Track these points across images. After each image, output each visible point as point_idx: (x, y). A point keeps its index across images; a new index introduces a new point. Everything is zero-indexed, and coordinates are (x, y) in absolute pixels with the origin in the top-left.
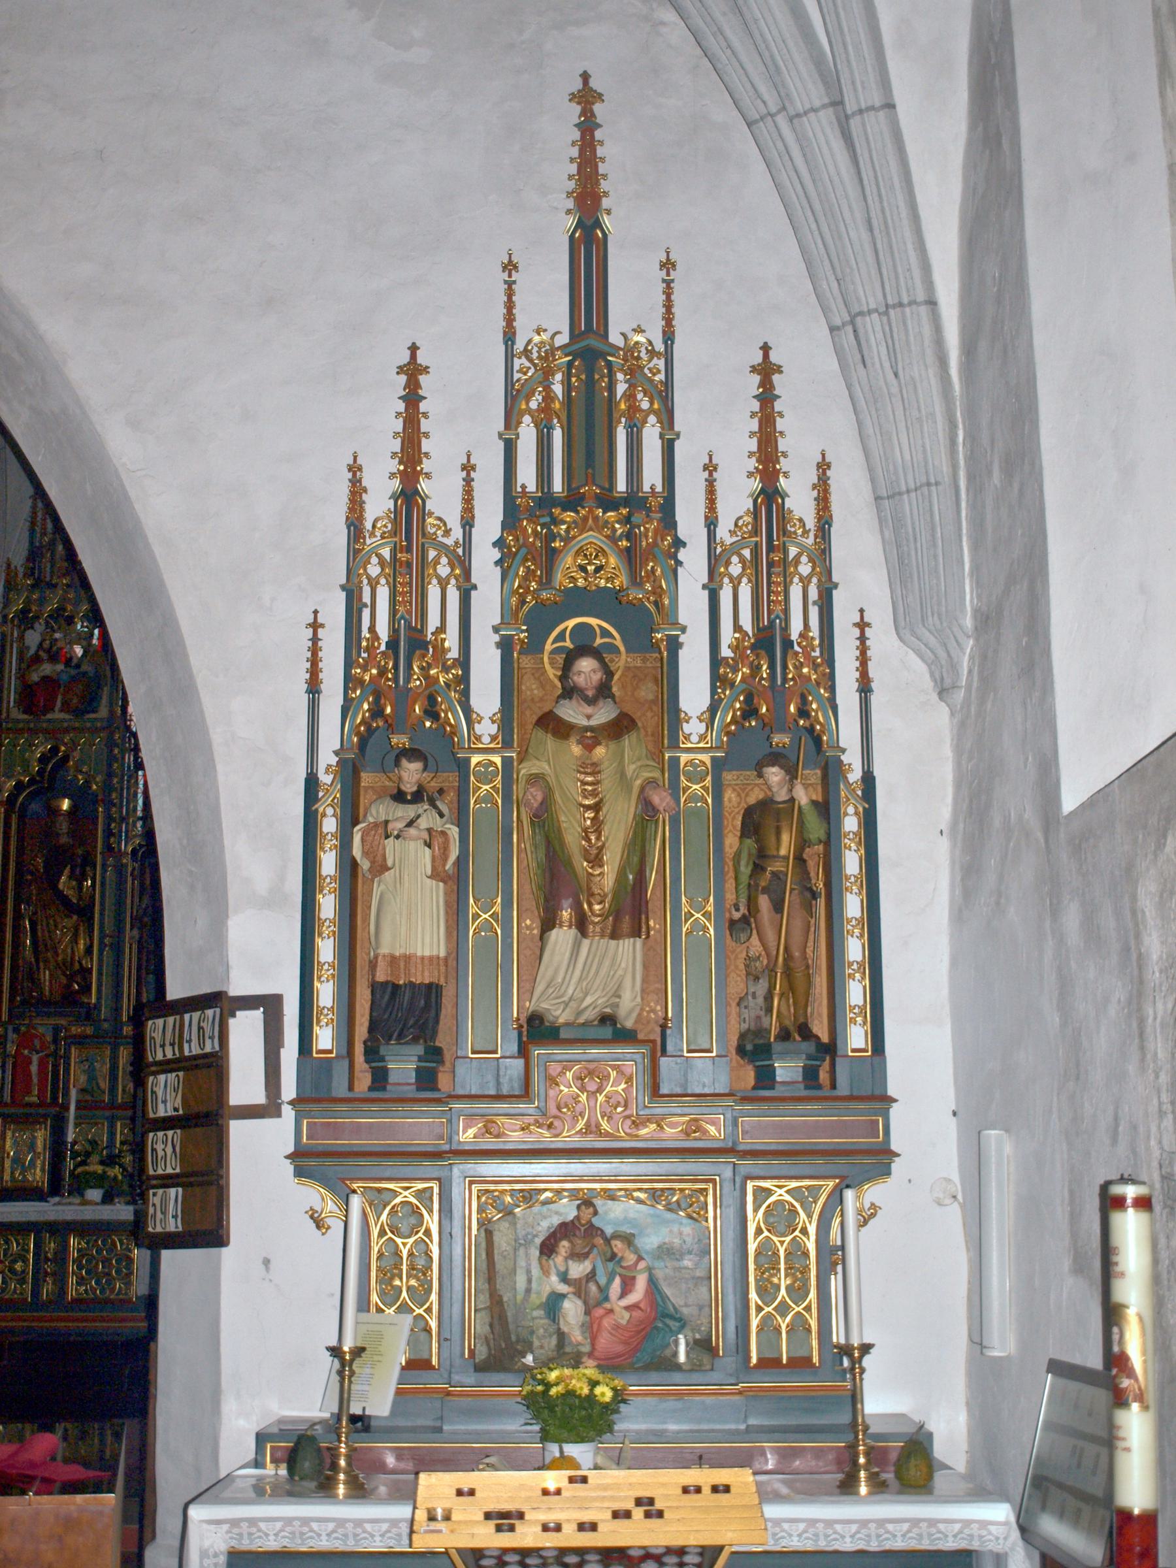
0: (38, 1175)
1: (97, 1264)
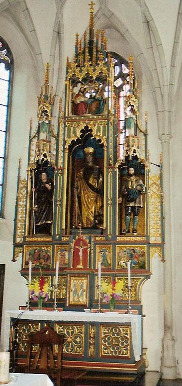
0: (85, 282)
1: (112, 340)
